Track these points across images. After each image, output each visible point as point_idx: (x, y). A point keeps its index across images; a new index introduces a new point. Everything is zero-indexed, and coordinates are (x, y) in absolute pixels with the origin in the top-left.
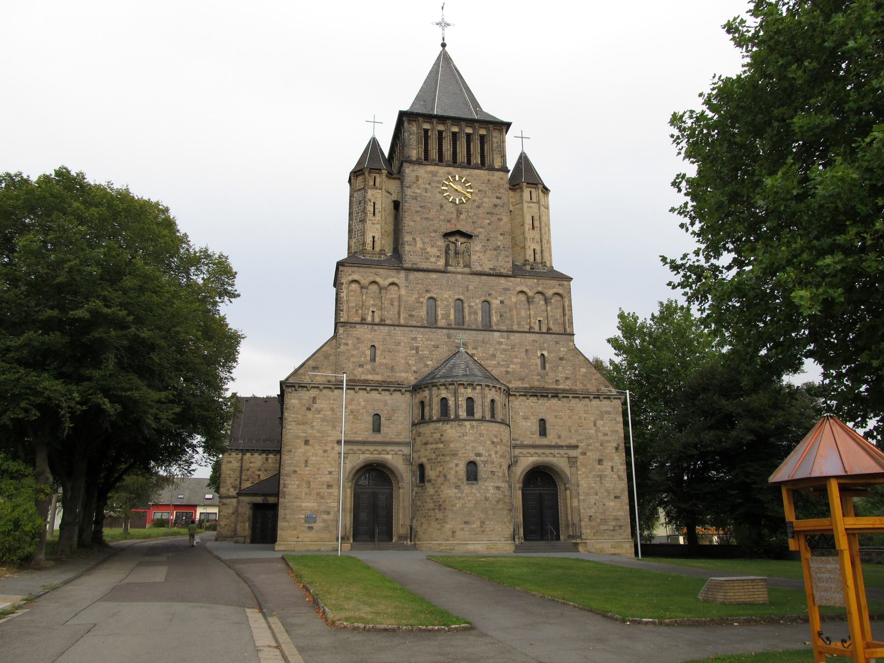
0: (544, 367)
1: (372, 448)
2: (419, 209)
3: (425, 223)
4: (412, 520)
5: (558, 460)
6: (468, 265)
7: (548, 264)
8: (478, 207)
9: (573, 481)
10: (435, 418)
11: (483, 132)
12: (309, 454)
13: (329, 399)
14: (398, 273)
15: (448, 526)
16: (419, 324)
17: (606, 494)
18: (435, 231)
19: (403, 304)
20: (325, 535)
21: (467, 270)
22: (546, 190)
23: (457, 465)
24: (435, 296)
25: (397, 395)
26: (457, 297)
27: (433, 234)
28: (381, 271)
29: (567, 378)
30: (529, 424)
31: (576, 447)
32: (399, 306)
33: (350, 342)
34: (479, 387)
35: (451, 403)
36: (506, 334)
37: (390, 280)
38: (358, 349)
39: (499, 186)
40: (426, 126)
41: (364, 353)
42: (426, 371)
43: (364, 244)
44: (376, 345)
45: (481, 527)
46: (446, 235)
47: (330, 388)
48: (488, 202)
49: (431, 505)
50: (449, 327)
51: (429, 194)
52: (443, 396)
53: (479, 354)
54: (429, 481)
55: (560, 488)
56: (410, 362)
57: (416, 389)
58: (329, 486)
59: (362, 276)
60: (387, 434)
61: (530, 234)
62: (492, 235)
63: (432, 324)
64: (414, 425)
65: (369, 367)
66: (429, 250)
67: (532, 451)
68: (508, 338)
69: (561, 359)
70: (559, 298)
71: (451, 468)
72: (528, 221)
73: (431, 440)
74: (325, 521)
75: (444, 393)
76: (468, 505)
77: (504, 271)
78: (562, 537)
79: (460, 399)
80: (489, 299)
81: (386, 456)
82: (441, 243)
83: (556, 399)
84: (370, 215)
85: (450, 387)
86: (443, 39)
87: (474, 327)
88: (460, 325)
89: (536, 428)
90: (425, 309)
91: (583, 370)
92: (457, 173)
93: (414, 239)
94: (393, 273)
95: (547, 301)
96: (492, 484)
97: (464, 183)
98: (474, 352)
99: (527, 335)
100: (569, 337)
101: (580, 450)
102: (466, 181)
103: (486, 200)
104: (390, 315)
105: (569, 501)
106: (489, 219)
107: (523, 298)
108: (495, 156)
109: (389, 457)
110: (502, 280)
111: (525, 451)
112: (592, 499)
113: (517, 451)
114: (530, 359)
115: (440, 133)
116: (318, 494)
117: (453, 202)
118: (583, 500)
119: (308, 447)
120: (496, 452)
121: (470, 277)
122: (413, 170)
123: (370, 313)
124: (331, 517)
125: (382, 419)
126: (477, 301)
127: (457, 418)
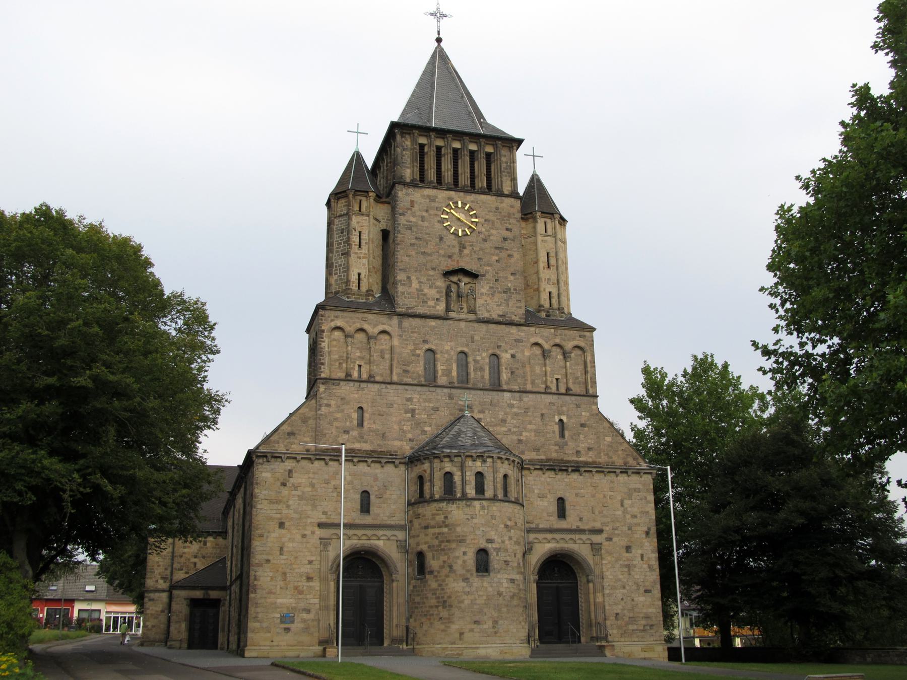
0: (562, 435)
1: (360, 532)
2: (414, 241)
3: (422, 259)
4: (408, 620)
5: (580, 547)
6: (472, 311)
7: (566, 311)
8: (485, 240)
9: (597, 572)
10: (437, 496)
11: (489, 149)
12: (284, 540)
13: (308, 473)
14: (390, 319)
15: (454, 627)
16: (415, 382)
17: (634, 587)
18: (434, 269)
19: (395, 356)
20: (305, 638)
21: (472, 316)
22: (563, 221)
23: (465, 553)
24: (434, 348)
25: (390, 468)
26: (459, 349)
27: (431, 273)
28: (370, 317)
29: (589, 449)
30: (546, 504)
31: (600, 531)
32: (392, 359)
33: (333, 403)
34: (489, 460)
35: (457, 478)
36: (517, 395)
37: (381, 328)
38: (343, 411)
39: (509, 216)
40: (423, 140)
41: (349, 416)
42: (424, 439)
43: (348, 282)
44: (364, 406)
45: (494, 627)
46: (447, 274)
47: (310, 459)
48: (496, 234)
49: (433, 602)
50: (450, 386)
51: (426, 224)
52: (448, 470)
53: (487, 418)
54: (431, 572)
55: (582, 580)
56: (405, 428)
57: (413, 460)
58: (309, 579)
59: (347, 322)
60: (378, 515)
61: (545, 274)
62: (501, 274)
63: (430, 381)
64: (410, 504)
65: (355, 433)
66: (426, 291)
67: (549, 536)
68: (521, 400)
69: (583, 425)
70: (579, 352)
71: (458, 558)
72: (543, 258)
73: (432, 523)
74: (304, 621)
75: (448, 467)
76: (478, 602)
77: (515, 319)
78: (583, 639)
79: (468, 474)
80: (498, 352)
81: (377, 542)
82: (441, 283)
83: (577, 473)
84: (355, 247)
85: (456, 459)
86: (439, 33)
87: (480, 386)
88: (464, 383)
89: (553, 508)
90: (422, 363)
91: (609, 439)
92: (459, 198)
93: (409, 278)
94: (383, 319)
95: (565, 355)
96: (506, 576)
97: (468, 211)
98: (481, 416)
99: (543, 396)
100: (592, 399)
101: (604, 535)
102: (471, 209)
103: (493, 232)
104: (380, 370)
105: (592, 596)
106: (497, 255)
107: (537, 350)
108: (504, 178)
109: (380, 543)
110: (514, 330)
111: (541, 536)
112: (619, 593)
113: (532, 536)
114: (546, 425)
115: (439, 149)
116: (296, 588)
117: (455, 234)
118: (610, 595)
119: (283, 531)
120: (510, 538)
121: (476, 325)
122: (407, 194)
123: (357, 368)
124: (311, 616)
125: (372, 497)
126: (484, 354)
127: (464, 497)
